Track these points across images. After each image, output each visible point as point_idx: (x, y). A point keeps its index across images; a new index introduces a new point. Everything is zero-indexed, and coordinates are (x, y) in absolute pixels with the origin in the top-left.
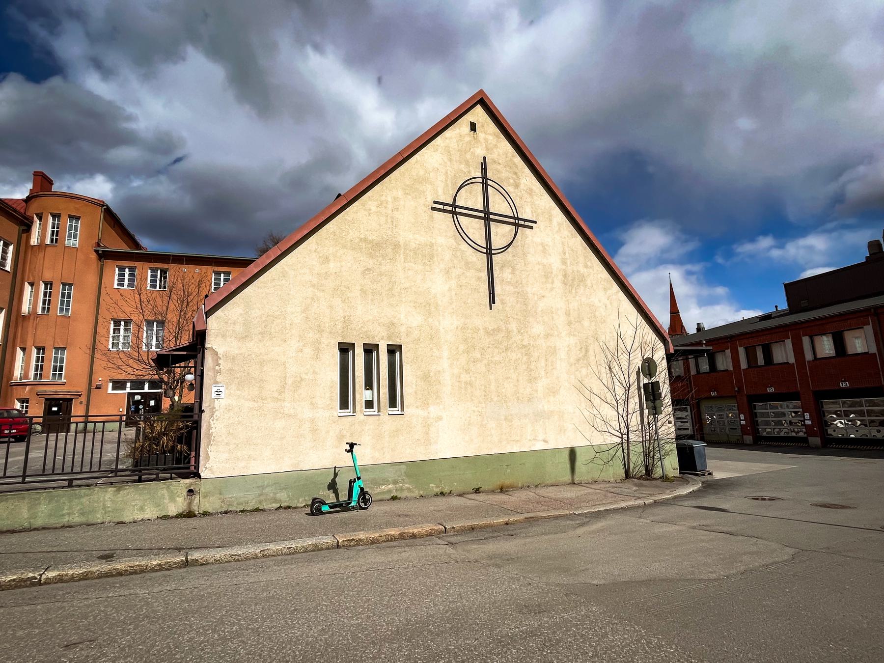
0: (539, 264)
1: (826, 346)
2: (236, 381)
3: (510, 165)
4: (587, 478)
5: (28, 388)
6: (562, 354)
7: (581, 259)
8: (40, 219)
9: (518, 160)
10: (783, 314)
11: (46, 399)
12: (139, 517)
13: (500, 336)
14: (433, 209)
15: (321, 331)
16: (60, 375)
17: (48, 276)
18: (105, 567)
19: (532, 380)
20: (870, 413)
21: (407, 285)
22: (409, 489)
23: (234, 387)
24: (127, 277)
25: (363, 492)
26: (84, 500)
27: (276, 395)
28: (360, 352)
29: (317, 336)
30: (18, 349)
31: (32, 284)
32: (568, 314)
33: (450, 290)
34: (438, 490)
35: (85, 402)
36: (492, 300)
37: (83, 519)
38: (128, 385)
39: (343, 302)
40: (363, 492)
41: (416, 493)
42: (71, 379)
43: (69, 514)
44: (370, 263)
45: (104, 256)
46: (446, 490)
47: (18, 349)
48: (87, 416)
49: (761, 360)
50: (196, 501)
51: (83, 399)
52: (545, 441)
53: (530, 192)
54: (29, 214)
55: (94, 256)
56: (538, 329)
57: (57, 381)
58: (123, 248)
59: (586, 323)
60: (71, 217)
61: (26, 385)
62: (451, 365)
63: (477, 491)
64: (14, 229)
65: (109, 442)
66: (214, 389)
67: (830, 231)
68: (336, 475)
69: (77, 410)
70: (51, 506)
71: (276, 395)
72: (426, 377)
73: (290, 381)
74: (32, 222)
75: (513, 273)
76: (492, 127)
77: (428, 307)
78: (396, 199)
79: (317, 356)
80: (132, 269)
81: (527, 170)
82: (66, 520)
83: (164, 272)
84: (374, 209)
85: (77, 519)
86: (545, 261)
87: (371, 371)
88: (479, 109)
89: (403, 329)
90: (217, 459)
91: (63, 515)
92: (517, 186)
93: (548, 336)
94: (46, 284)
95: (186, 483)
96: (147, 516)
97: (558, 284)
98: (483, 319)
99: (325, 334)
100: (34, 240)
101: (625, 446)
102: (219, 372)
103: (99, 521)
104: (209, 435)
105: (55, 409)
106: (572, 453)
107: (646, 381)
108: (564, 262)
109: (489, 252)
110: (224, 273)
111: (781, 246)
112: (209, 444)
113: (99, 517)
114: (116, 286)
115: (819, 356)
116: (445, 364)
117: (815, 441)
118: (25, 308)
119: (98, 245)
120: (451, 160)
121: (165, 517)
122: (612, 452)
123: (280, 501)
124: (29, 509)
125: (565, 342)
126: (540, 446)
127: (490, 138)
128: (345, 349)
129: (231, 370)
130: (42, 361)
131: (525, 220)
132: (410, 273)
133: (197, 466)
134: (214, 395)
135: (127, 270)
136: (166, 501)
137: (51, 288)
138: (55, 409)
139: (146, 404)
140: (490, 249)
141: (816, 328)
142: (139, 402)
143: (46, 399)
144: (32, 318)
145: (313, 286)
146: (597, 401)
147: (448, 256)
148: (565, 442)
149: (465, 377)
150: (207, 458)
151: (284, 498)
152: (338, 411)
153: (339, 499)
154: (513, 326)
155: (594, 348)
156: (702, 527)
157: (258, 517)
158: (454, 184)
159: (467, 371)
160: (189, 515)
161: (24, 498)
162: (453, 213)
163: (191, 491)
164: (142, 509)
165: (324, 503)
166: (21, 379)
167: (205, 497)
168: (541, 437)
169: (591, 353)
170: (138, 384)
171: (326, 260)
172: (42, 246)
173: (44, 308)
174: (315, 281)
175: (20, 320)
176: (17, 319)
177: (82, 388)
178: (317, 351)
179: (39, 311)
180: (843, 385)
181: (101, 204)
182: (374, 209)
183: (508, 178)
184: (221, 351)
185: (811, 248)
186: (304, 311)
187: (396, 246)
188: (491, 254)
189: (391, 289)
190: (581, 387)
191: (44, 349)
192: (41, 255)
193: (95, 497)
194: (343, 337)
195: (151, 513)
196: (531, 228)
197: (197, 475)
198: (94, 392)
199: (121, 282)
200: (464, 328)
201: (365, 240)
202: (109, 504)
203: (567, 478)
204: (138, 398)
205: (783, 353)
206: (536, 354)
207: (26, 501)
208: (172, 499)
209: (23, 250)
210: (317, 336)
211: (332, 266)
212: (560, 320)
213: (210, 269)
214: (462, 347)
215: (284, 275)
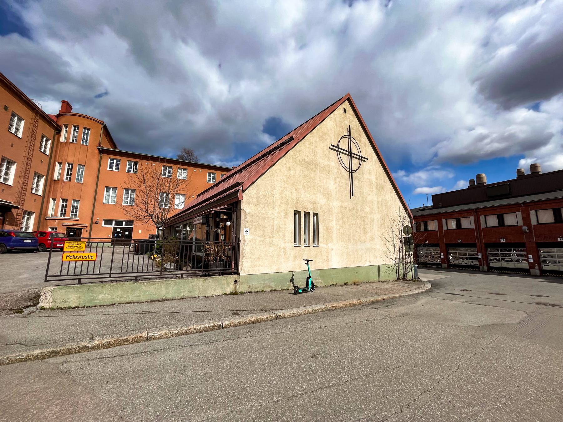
0: (368, 179)
1: (453, 224)
2: (254, 227)
3: (358, 131)
4: (384, 279)
5: (57, 221)
6: (376, 222)
7: (383, 178)
8: (66, 127)
9: (361, 128)
10: (429, 208)
11: (67, 228)
12: (214, 294)
13: (354, 212)
14: (330, 148)
15: (287, 203)
16: (76, 215)
17: (70, 160)
18: (236, 320)
19: (365, 233)
20: (459, 254)
21: (320, 184)
22: (321, 283)
23: (253, 229)
24: (115, 165)
25: (312, 284)
26: (190, 285)
27: (270, 234)
28: (302, 215)
29: (286, 206)
30: (51, 200)
31: (60, 164)
32: (378, 203)
33: (336, 188)
34: (331, 283)
35: (88, 231)
36: (352, 193)
37: (190, 295)
38: (114, 223)
39: (296, 190)
40: (312, 284)
41: (324, 285)
42: (82, 218)
43: (184, 292)
44: (306, 172)
45: (102, 152)
46: (335, 284)
47: (51, 200)
48: (89, 238)
49: (422, 229)
50: (238, 287)
51: (88, 229)
52: (370, 262)
53: (365, 144)
54: (59, 124)
55: (97, 151)
56: (367, 209)
57: (73, 218)
58: (109, 148)
59: (384, 208)
60: (85, 128)
61: (55, 219)
62: (336, 224)
63: (346, 284)
64: (50, 132)
65: (118, 253)
66: (245, 230)
67: (428, 171)
68: (293, 275)
69: (85, 234)
70: (175, 288)
71: (270, 234)
72: (327, 229)
73: (275, 228)
74: (62, 129)
75: (359, 182)
76: (351, 112)
77: (328, 196)
78: (316, 142)
79: (286, 217)
80: (118, 161)
81: (364, 134)
82: (182, 295)
83: (136, 164)
84: (308, 146)
85: (187, 295)
86: (370, 178)
87: (306, 224)
88: (347, 102)
89: (319, 206)
90: (246, 266)
91: (181, 292)
92: (360, 141)
93: (371, 213)
94: (69, 164)
95: (234, 277)
96: (217, 294)
97: (374, 189)
98: (348, 203)
99: (289, 206)
100: (62, 139)
101: (397, 265)
102: (247, 221)
103: (197, 296)
104: (243, 253)
105: (72, 234)
106: (379, 267)
107: (405, 236)
108: (377, 179)
109: (351, 171)
110: (169, 167)
111: (407, 176)
112: (243, 258)
113: (197, 294)
114: (108, 169)
115: (449, 228)
116: (334, 223)
117: (445, 265)
118: (56, 177)
119: (99, 145)
120: (336, 125)
121: (225, 294)
122: (392, 268)
123: (272, 287)
124: (166, 289)
125: (377, 216)
126: (368, 264)
127: (351, 117)
128: (297, 213)
129: (252, 221)
130: (66, 207)
131: (364, 158)
132: (322, 179)
133: (238, 269)
134: (245, 233)
135: (115, 161)
136: (225, 286)
137: (72, 167)
138: (72, 234)
139: (123, 233)
140: (352, 170)
141: (448, 216)
142: (118, 232)
143: (67, 228)
144: (60, 183)
145: (284, 181)
146: (388, 244)
147: (335, 171)
148: (377, 263)
149: (341, 231)
150: (242, 265)
151: (273, 285)
152: (293, 244)
153: (302, 288)
154: (359, 208)
155: (387, 220)
156: (463, 302)
157: (260, 296)
158: (338, 137)
159: (342, 227)
160: (235, 293)
161: (163, 283)
162: (352, 153)
163: (236, 281)
164: (215, 290)
165: (299, 288)
166: (52, 216)
167: (242, 284)
168: (368, 260)
169: (386, 222)
170: (119, 223)
171: (289, 169)
172: (67, 143)
173: (67, 178)
174: (285, 179)
175: (53, 183)
176: (51, 182)
177: (87, 222)
178: (286, 214)
179: (65, 179)
180: (459, 241)
181: (102, 123)
182: (308, 146)
183: (357, 137)
184: (247, 211)
185: (420, 178)
186: (281, 194)
187: (316, 165)
188: (352, 173)
189: (314, 186)
190: (382, 238)
191: (67, 200)
192: (66, 148)
193: (195, 283)
194: (296, 208)
195: (219, 292)
196: (365, 161)
197: (238, 274)
198: (94, 225)
199: (111, 166)
200: (341, 207)
201: (304, 160)
202: (201, 287)
203: (377, 279)
204: (118, 230)
205: (433, 226)
206: (366, 221)
207: (164, 285)
208: (228, 285)
209: (56, 144)
210: (286, 206)
211: (292, 172)
212: (375, 205)
213: (161, 164)
214: (340, 216)
215: (273, 175)
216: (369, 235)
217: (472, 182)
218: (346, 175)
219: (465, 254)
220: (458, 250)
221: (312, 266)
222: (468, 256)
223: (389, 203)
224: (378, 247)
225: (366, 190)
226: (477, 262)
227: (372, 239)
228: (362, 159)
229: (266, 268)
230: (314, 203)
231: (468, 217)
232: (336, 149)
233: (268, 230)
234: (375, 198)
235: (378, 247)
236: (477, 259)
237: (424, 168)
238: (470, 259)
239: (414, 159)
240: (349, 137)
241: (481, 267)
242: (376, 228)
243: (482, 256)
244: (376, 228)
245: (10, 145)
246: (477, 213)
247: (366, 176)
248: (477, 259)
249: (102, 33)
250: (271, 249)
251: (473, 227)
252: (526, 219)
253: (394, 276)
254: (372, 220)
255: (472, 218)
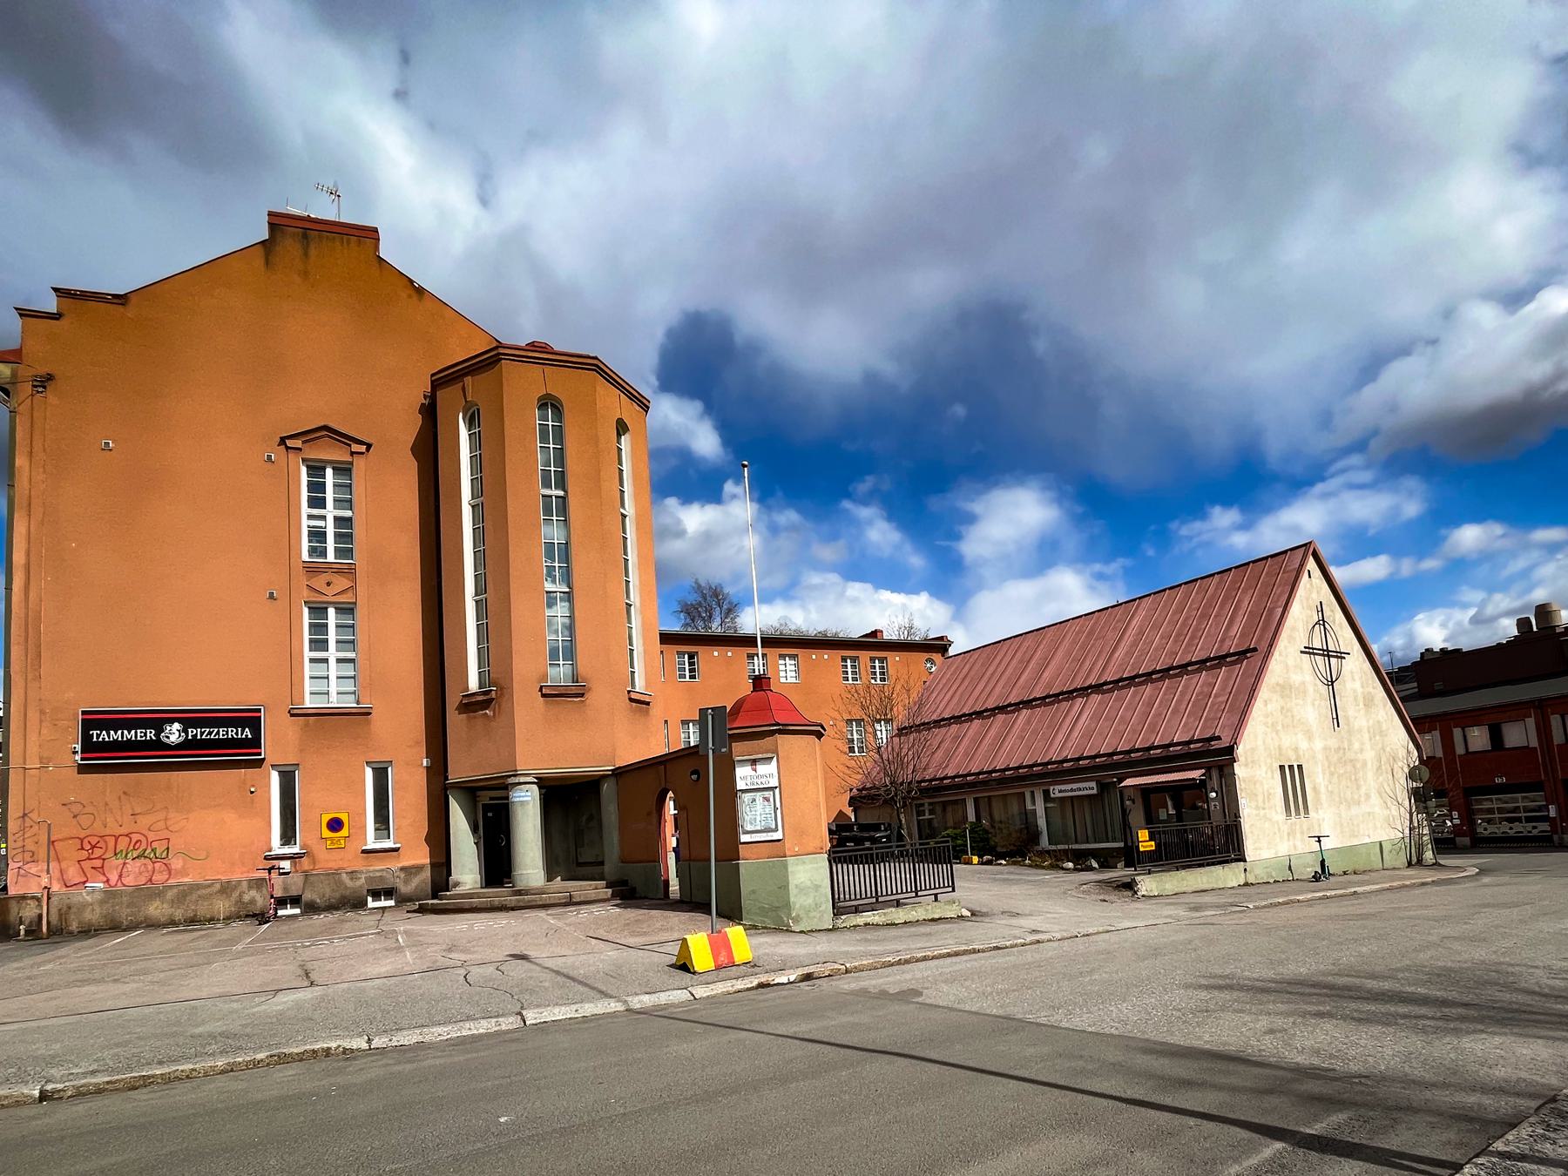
19: (1358, 788)
56: (1356, 746)
67: (1326, 496)
77: (1309, 736)
111: (1245, 526)
117: (1466, 840)
125: (1369, 755)
126: (1367, 840)
128: (1282, 767)
160: (1246, 884)
212: (1366, 736)
216: (1363, 791)
217: (1523, 624)
218: (1324, 689)
219: (1516, 810)
220: (1492, 802)
221: (1327, 844)
222: (1523, 815)
223: (1384, 727)
224: (1377, 810)
225: (1351, 713)
226: (1545, 826)
227: (1368, 796)
228: (1340, 656)
229: (1266, 854)
230: (1296, 750)
231: (1521, 718)
232: (1309, 651)
233: (1260, 798)
234: (1364, 723)
235: (1377, 810)
236: (1546, 819)
237: (1310, 483)
238: (1529, 820)
239: (1274, 448)
240: (1322, 622)
241: (1556, 837)
242: (1370, 775)
243: (1559, 810)
244: (1370, 775)
245: (1316, 779)
246: (1541, 708)
247: (1349, 685)
248: (1546, 819)
249: (971, 519)
250: (1267, 825)
251: (1534, 743)
252: (1496, 736)
253: (1403, 860)
254: (1365, 764)
255: (1531, 722)
